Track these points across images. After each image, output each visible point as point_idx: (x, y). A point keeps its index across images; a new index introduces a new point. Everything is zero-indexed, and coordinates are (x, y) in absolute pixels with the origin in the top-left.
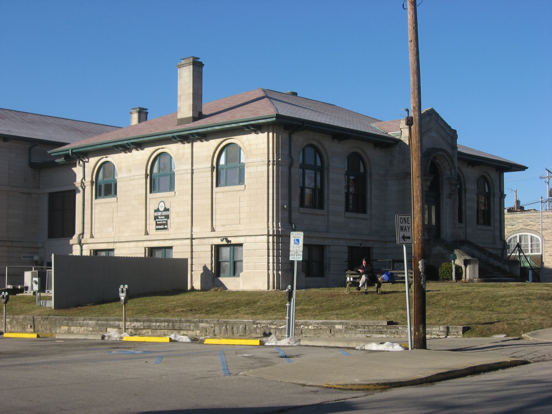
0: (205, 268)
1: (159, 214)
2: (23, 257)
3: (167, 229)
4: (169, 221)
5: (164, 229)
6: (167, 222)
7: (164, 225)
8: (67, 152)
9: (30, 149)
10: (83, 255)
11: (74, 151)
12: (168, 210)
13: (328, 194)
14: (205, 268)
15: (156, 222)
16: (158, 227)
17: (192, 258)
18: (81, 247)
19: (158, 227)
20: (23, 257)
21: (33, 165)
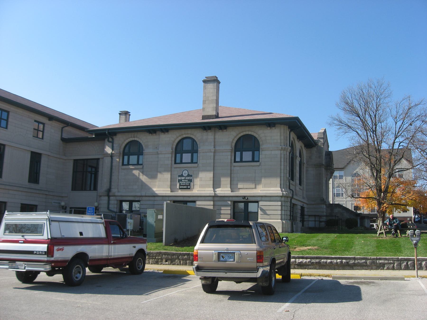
0: (229, 299)
1: (183, 178)
2: (54, 202)
3: (190, 188)
4: (192, 184)
5: (187, 188)
6: (190, 184)
7: (187, 186)
8: (105, 131)
9: (62, 128)
10: (250, 153)
11: (110, 131)
12: (191, 176)
13: (172, 157)
14: (229, 299)
15: (180, 184)
16: (181, 187)
17: (231, 163)
18: (109, 198)
19: (181, 187)
20: (54, 202)
21: (63, 140)
